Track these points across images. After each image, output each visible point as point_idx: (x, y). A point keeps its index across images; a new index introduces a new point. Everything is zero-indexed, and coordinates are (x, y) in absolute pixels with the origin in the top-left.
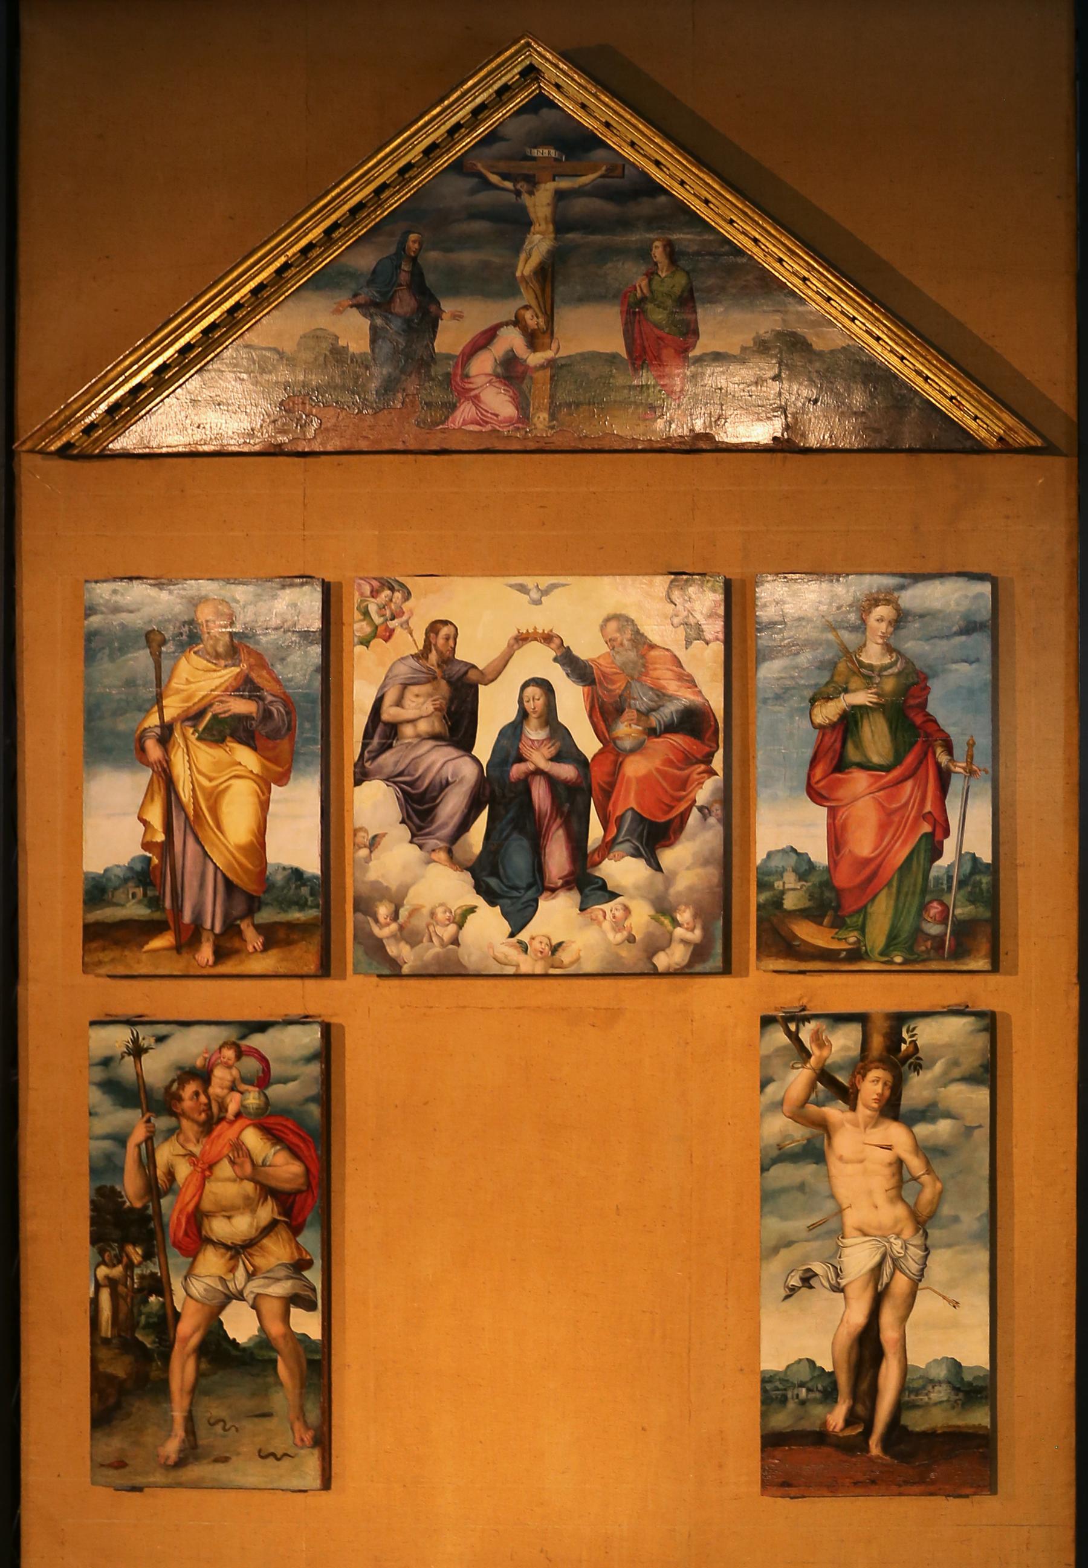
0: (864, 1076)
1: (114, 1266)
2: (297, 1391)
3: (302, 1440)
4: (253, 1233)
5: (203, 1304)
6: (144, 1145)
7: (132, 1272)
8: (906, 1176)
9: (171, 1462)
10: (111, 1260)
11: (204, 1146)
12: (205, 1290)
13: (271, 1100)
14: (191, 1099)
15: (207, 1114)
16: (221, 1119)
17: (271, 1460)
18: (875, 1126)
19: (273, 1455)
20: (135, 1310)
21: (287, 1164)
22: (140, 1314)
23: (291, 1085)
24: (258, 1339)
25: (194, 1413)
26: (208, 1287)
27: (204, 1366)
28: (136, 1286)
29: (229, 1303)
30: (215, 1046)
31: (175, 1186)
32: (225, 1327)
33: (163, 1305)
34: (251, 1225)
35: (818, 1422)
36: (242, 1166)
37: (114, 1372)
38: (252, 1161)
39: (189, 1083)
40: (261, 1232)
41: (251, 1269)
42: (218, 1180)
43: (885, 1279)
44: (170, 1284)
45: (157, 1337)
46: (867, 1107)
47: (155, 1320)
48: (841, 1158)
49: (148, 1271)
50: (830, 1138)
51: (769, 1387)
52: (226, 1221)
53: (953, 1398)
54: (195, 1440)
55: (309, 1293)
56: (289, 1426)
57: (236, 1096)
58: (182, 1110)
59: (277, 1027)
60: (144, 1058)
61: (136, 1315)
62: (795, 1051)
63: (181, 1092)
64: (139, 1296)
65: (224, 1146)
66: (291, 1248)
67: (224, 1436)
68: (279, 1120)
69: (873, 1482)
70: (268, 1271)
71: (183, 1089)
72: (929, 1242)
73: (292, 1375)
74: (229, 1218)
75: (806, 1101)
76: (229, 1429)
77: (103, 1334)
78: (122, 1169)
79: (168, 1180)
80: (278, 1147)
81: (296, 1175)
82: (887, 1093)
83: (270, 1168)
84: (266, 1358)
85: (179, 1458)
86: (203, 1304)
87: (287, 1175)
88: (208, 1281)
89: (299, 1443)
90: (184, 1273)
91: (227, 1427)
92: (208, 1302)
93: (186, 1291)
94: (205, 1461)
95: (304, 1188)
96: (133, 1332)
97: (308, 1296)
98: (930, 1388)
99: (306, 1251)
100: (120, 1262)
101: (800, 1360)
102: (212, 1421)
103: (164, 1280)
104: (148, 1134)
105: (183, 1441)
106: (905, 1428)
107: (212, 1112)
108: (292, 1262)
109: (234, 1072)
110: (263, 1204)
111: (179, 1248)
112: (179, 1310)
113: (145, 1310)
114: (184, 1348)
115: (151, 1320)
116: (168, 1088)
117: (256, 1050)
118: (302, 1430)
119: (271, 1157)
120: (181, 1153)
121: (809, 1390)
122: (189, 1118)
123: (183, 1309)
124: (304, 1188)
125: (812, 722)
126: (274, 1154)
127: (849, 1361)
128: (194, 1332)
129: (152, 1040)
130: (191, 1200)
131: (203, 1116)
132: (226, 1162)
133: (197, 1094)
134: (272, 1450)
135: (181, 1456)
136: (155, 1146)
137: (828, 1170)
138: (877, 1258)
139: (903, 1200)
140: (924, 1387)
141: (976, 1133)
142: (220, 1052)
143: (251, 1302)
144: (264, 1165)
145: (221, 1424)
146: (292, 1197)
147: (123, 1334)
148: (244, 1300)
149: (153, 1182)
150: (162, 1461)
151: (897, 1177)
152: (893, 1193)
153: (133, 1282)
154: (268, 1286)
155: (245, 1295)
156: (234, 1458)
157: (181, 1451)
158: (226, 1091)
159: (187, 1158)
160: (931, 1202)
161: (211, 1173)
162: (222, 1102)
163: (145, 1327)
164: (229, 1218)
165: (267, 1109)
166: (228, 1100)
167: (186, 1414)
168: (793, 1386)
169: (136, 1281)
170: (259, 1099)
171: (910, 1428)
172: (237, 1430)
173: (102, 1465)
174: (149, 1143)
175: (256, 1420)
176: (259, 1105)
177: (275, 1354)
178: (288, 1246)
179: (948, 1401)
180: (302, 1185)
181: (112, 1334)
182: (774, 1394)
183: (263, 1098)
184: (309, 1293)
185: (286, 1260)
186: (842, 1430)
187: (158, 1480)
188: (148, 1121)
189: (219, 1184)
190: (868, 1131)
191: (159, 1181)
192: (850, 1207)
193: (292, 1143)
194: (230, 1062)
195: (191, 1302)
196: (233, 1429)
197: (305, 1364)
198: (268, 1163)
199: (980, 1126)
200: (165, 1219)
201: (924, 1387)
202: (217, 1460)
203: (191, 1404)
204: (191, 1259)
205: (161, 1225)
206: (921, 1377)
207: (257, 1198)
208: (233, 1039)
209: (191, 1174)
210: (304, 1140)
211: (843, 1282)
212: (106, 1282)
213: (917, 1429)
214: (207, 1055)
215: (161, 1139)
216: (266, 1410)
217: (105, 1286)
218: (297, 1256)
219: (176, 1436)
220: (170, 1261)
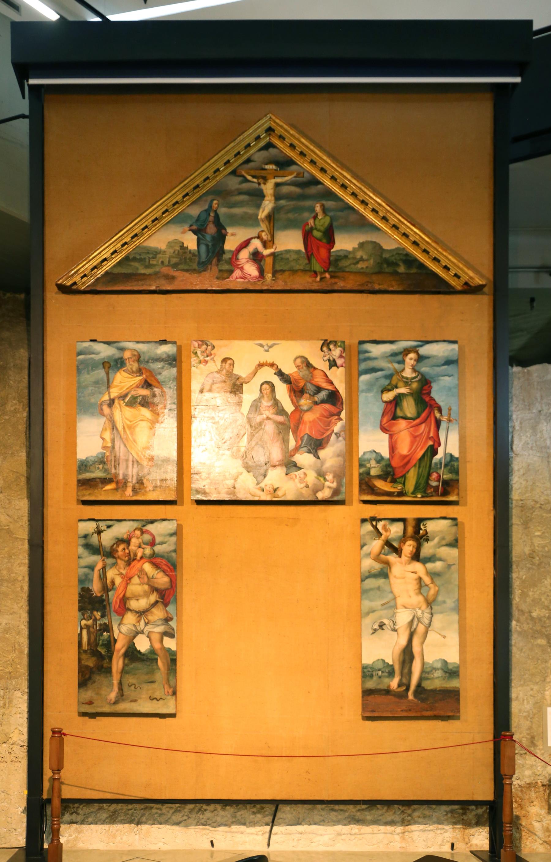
0: (404, 543)
1: (89, 620)
2: (166, 672)
3: (168, 692)
4: (148, 606)
8: (423, 584)
9: (112, 702)
16: (134, 560)
18: (409, 563)
19: (156, 699)
20: (98, 638)
23: (164, 546)
27: (126, 662)
30: (132, 530)
31: (114, 587)
32: (136, 645)
33: (109, 636)
34: (147, 603)
35: (386, 685)
36: (143, 578)
42: (133, 584)
43: (414, 626)
46: (406, 556)
48: (395, 577)
50: (390, 569)
51: (365, 670)
53: (444, 675)
55: (172, 631)
56: (162, 686)
57: (141, 550)
60: (102, 534)
62: (375, 533)
64: (99, 632)
67: (135, 691)
69: (410, 710)
70: (154, 622)
72: (433, 611)
74: (138, 600)
75: (380, 553)
77: (84, 648)
78: (92, 580)
82: (414, 550)
86: (127, 636)
90: (118, 623)
93: (119, 630)
96: (97, 647)
98: (434, 671)
100: (91, 618)
101: (378, 660)
103: (110, 626)
105: (118, 693)
106: (423, 688)
112: (116, 638)
113: (102, 638)
114: (118, 654)
115: (104, 643)
121: (383, 672)
122: (121, 559)
124: (170, 587)
127: (399, 660)
128: (122, 648)
129: (106, 527)
132: (136, 577)
133: (124, 549)
134: (155, 697)
137: (390, 582)
138: (411, 618)
139: (421, 594)
140: (431, 671)
141: (453, 567)
144: (152, 578)
151: (419, 585)
152: (417, 591)
154: (154, 628)
156: (139, 701)
157: (116, 697)
158: (137, 548)
160: (434, 595)
163: (101, 646)
164: (138, 600)
167: (119, 682)
168: (376, 670)
171: (426, 688)
173: (83, 703)
175: (149, 684)
179: (442, 677)
182: (367, 673)
183: (152, 551)
184: (172, 631)
186: (397, 689)
190: (407, 566)
192: (399, 596)
195: (121, 635)
199: (454, 564)
200: (110, 601)
201: (431, 671)
202: (132, 701)
203: (121, 677)
206: (430, 667)
208: (140, 527)
209: (122, 582)
211: (396, 627)
213: (429, 688)
216: (152, 680)
220: (113, 618)
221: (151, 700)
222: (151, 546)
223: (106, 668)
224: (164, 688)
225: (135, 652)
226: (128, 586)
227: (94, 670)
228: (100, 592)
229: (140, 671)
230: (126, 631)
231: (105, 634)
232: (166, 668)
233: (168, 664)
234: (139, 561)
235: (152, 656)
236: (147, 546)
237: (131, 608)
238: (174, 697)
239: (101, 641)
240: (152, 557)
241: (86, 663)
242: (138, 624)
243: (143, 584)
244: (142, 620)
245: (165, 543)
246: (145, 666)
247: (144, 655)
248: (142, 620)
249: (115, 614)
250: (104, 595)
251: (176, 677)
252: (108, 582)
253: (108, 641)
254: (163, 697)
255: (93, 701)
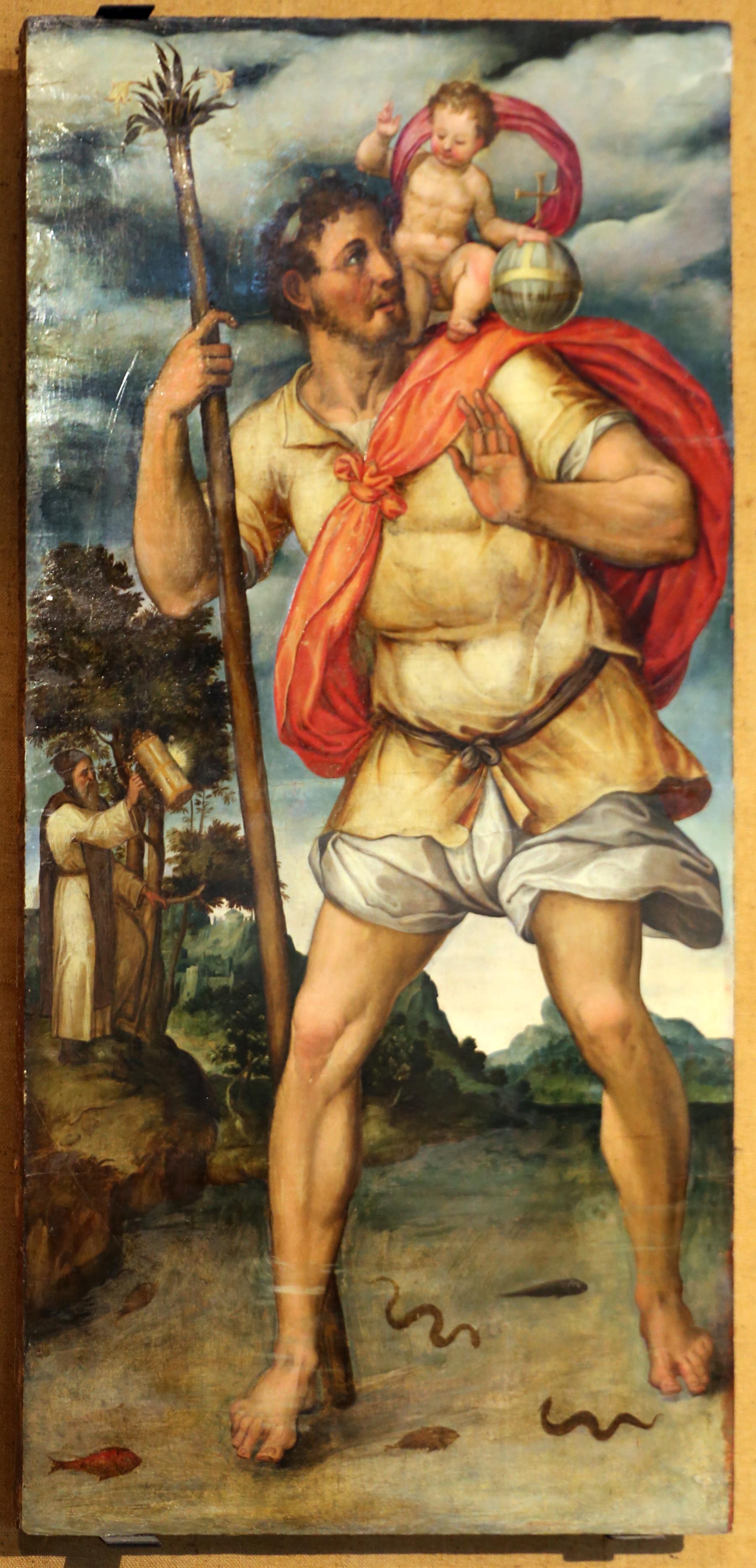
1: (103, 805)
2: (661, 1208)
3: (675, 1370)
4: (528, 699)
5: (376, 928)
6: (196, 417)
7: (159, 824)
9: (273, 1449)
10: (92, 786)
11: (382, 418)
12: (383, 882)
13: (585, 271)
14: (342, 266)
15: (389, 315)
16: (434, 332)
17: (581, 1435)
19: (586, 1419)
20: (167, 951)
21: (636, 472)
22: (183, 961)
23: (643, 224)
24: (543, 1042)
25: (344, 1286)
26: (390, 873)
27: (374, 1132)
28: (168, 871)
29: (456, 923)
30: (418, 100)
31: (290, 544)
32: (443, 1002)
33: (253, 932)
34: (522, 671)
36: (496, 478)
37: (101, 1155)
38: (529, 469)
39: (335, 219)
40: (553, 694)
41: (521, 812)
42: (420, 526)
44: (274, 866)
45: (231, 1038)
47: (230, 981)
49: (208, 824)
52: (445, 656)
54: (348, 1376)
55: (701, 890)
56: (633, 1321)
57: (482, 256)
58: (317, 303)
59: (601, 42)
60: (199, 135)
61: (168, 964)
63: (312, 246)
64: (179, 905)
65: (443, 418)
66: (642, 743)
67: (438, 1362)
68: (610, 335)
70: (574, 819)
71: (318, 238)
73: (644, 1158)
74: (455, 646)
76: (452, 1338)
77: (66, 1031)
78: (130, 494)
79: (270, 526)
80: (606, 421)
81: (660, 507)
83: (585, 487)
84: (564, 1101)
85: (299, 1435)
86: (376, 928)
87: (632, 510)
88: (391, 851)
89: (667, 1382)
90: (318, 826)
91: (445, 1334)
92: (392, 923)
93: (322, 883)
94: (378, 1446)
95: (685, 550)
96: (160, 1024)
97: (696, 897)
99: (687, 753)
100: (120, 794)
102: (399, 1312)
103: (257, 852)
104: (212, 380)
105: (312, 1380)
107: (405, 310)
108: (646, 789)
109: (474, 180)
110: (559, 602)
111: (303, 746)
112: (301, 946)
113: (197, 948)
114: (315, 1072)
115: (216, 983)
116: (272, 236)
117: (537, 110)
118: (676, 1339)
119: (585, 452)
120: (310, 441)
122: (334, 328)
123: (313, 942)
124: (685, 550)
125: (488, 381)
126: (596, 441)
128: (347, 1022)
129: (226, 78)
130: (339, 592)
131: (379, 320)
132: (446, 466)
133: (358, 250)
134: (581, 1405)
135: (305, 1428)
136: (232, 417)
142: (430, 117)
143: (521, 915)
144: (562, 477)
145: (428, 1321)
146: (649, 576)
147: (129, 1029)
148: (501, 913)
149: (221, 532)
150: (247, 1447)
153: (161, 862)
154: (576, 865)
155: (504, 896)
156: (466, 1435)
157: (303, 1413)
158: (448, 242)
159: (329, 454)
161: (402, 504)
162: (438, 277)
163: (193, 1007)
164: (455, 646)
165: (572, 298)
166: (455, 267)
167: (318, 1290)
169: (169, 854)
170: (549, 265)
172: (476, 1341)
173: (60, 1465)
174: (214, 406)
175: (535, 1305)
176: (550, 284)
177: (595, 1089)
178: (631, 739)
180: (679, 538)
181: (93, 1031)
183: (560, 265)
184: (701, 890)
185: (628, 784)
187: (233, 1510)
188: (211, 338)
189: (427, 539)
191: (243, 530)
193: (645, 406)
194: (462, 151)
195: (335, 919)
196: (464, 1335)
197: (683, 1120)
198: (575, 473)
200: (260, 654)
202: (411, 1443)
203: (335, 1256)
204: (339, 783)
205: (249, 672)
207: (542, 583)
208: (470, 78)
209: (341, 508)
210: (681, 394)
212: (78, 859)
214: (390, 129)
215: (248, 398)
216: (562, 1273)
217: (74, 872)
218: (660, 772)
219: (289, 1362)
220: (277, 790)
221: (552, 1429)
222: (549, 227)
223: (225, 1187)
224: (645, 1334)
225: (441, 1060)
226: (390, 544)
227: (143, 1196)
228: (186, 587)
229: (475, 1205)
230: (375, 892)
231: (220, 912)
232: (662, 1180)
233: (673, 1146)
234: (465, 343)
235: (558, 1084)
236: (521, 232)
237: (410, 716)
238: (716, 1406)
239: (191, 975)
240: (559, 314)
241: (86, 1148)
242: (462, 834)
243: (495, 524)
244: (491, 800)
245: (650, 205)
246: (511, 1170)
247: (500, 1076)
248: (491, 800)
249: (293, 756)
250: (217, 606)
251: (730, 1247)
252: (244, 504)
253: (240, 971)
254: (635, 1411)
255: (137, 1449)
